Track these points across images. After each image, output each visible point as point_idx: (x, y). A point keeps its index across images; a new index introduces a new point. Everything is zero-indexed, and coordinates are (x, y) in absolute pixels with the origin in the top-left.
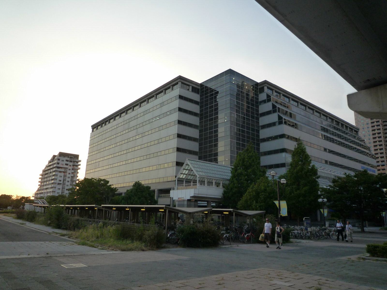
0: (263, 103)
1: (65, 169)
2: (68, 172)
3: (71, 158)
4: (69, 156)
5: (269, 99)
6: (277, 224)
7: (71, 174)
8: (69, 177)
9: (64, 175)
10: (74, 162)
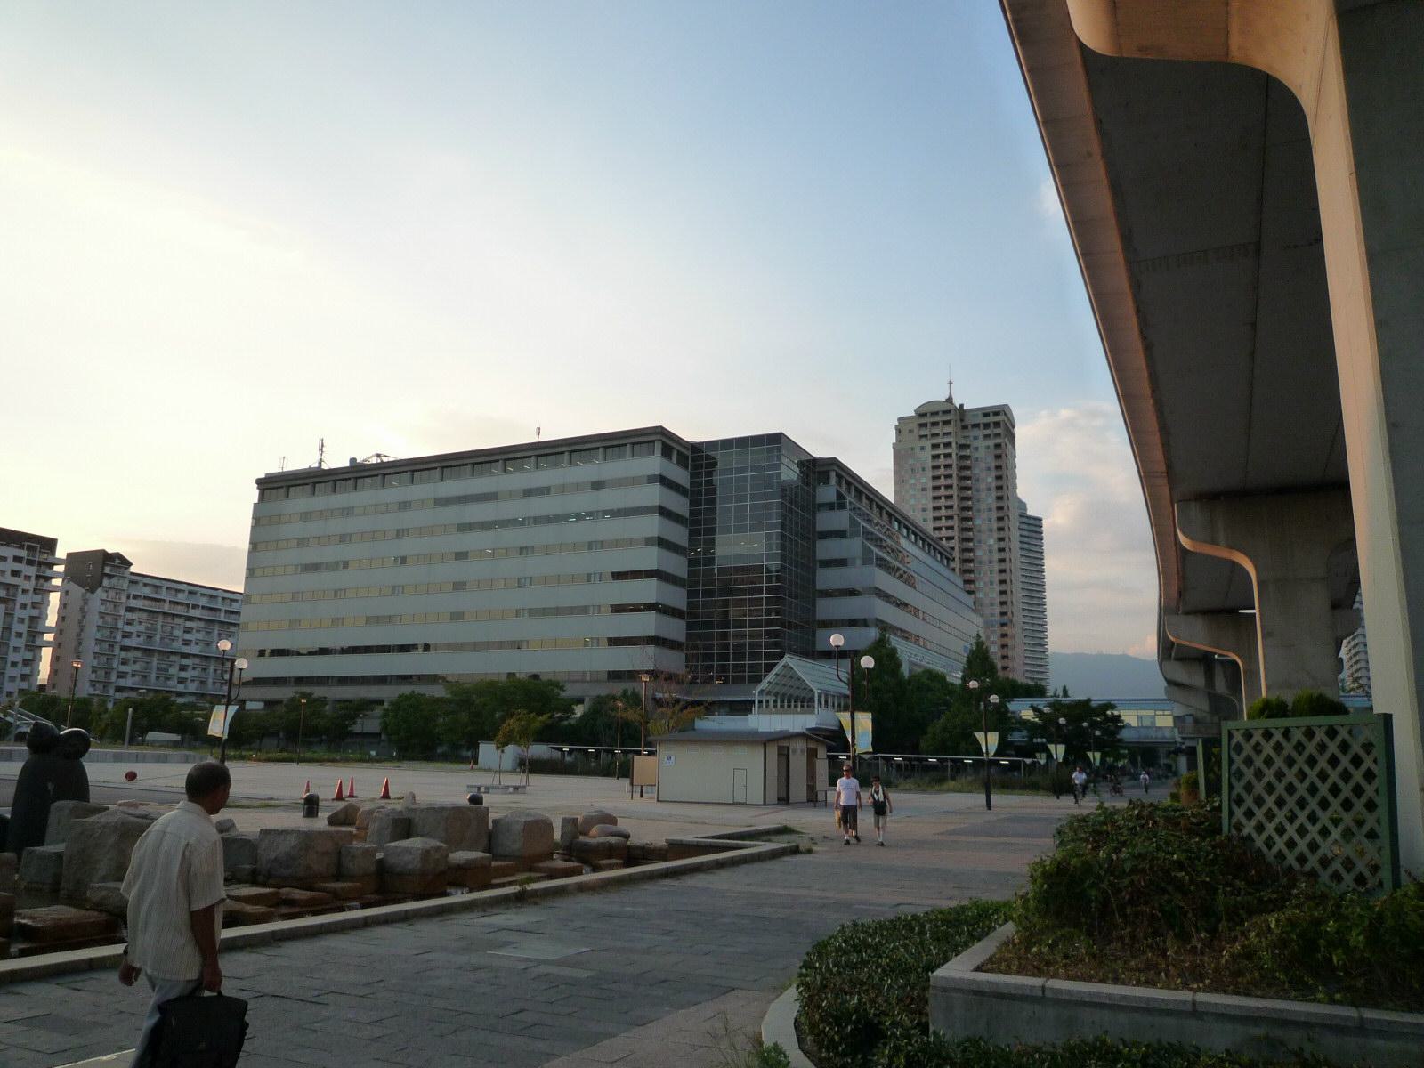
0: (1094, 704)
1: (8, 589)
2: (21, 599)
3: (30, 548)
4: (26, 543)
7: (28, 607)
8: (22, 620)
9: (6, 609)
10: (40, 564)
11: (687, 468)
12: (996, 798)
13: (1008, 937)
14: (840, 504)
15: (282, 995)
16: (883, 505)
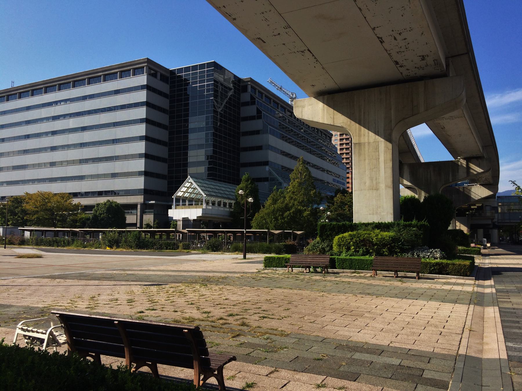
5: (253, 102)
6: (399, 252)
11: (168, 84)
12: (248, 256)
13: (487, 344)
14: (253, 102)
15: (69, 282)
16: (278, 102)
